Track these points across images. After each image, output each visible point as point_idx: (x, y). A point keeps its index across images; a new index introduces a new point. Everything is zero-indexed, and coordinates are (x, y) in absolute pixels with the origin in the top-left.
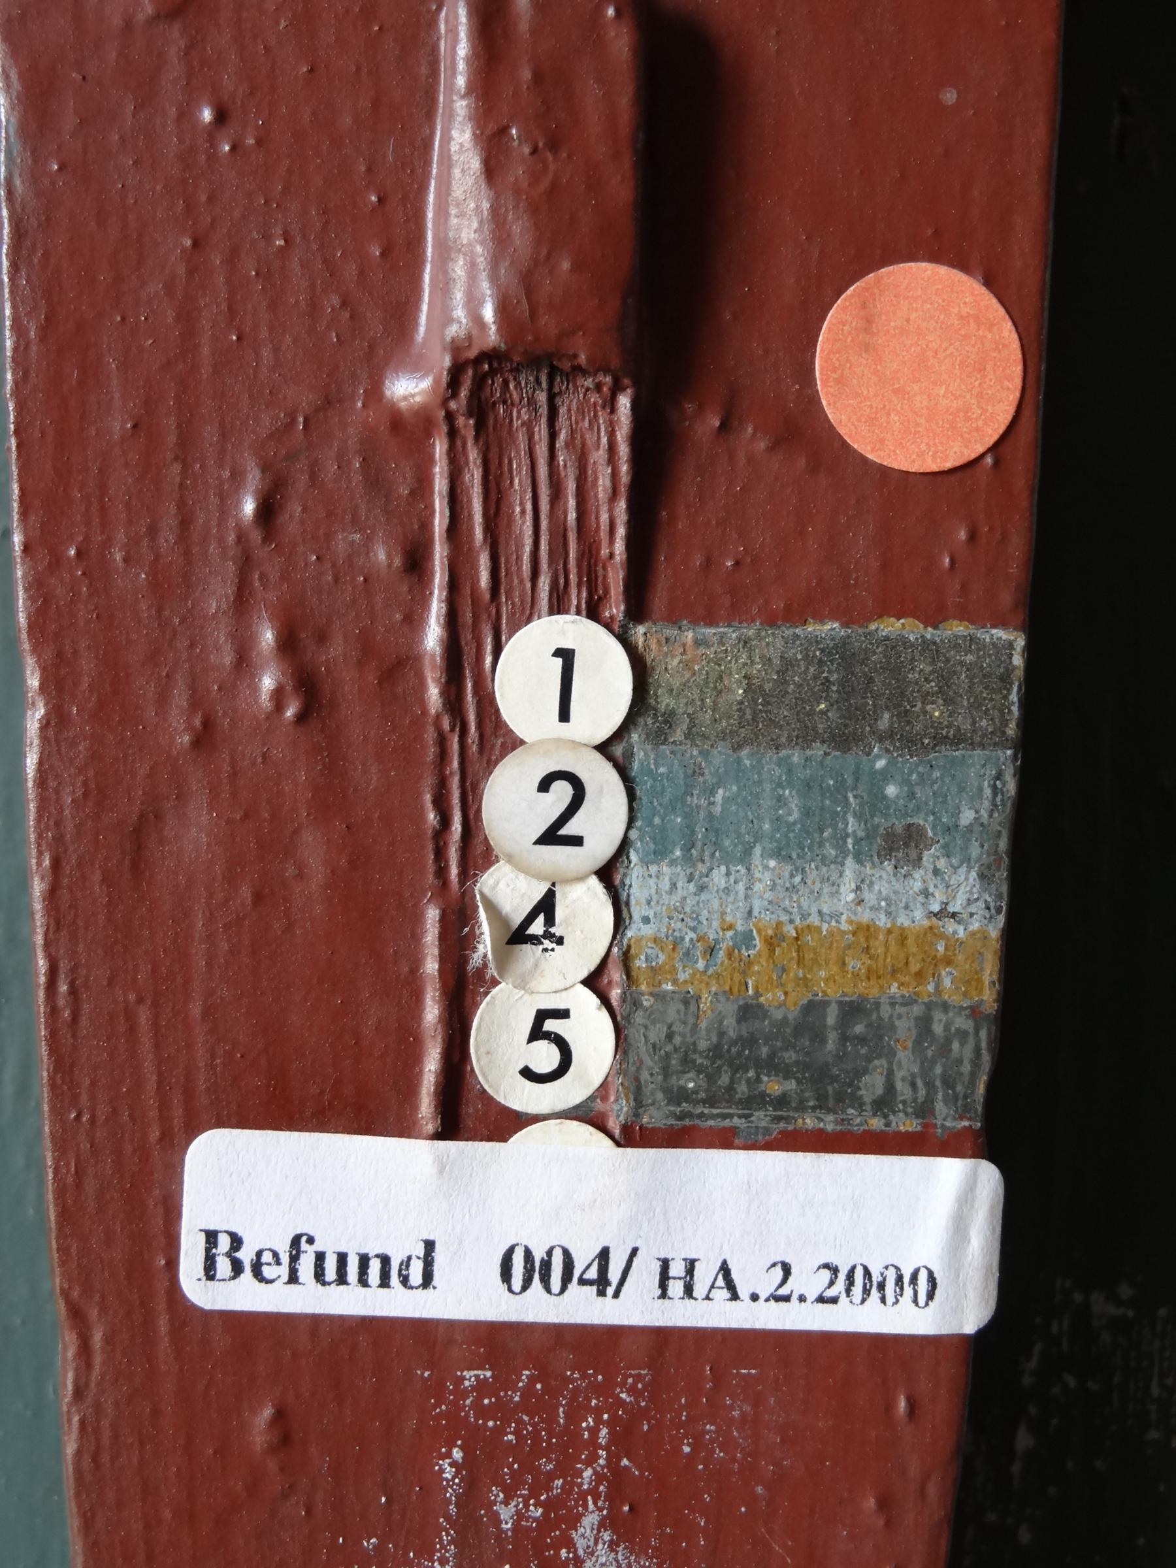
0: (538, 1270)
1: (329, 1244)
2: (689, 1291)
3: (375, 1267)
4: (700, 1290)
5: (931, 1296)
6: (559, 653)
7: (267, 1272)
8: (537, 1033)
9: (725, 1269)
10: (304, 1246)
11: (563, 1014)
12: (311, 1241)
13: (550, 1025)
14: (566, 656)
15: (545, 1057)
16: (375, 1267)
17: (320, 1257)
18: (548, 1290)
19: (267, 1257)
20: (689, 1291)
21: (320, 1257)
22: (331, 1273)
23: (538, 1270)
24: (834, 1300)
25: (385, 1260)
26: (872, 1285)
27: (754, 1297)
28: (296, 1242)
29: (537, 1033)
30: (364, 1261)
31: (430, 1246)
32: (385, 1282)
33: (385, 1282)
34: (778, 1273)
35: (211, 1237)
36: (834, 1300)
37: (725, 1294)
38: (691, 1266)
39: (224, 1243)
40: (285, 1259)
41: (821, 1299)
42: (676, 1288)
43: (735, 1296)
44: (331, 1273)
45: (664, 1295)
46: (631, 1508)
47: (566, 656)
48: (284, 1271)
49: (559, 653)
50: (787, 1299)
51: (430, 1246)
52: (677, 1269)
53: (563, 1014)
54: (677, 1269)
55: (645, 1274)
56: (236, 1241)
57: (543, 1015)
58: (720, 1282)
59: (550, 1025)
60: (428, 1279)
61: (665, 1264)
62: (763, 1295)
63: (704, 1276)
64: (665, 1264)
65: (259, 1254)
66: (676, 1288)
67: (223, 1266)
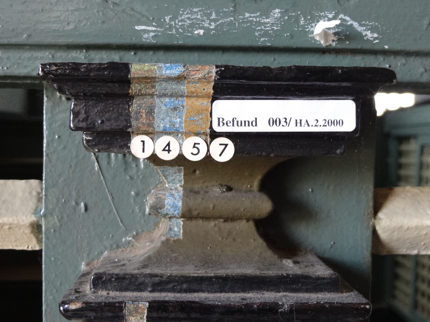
0: (275, 122)
1: (239, 119)
2: (301, 126)
3: (247, 123)
4: (303, 124)
5: (269, 120)
6: (142, 141)
7: (229, 124)
8: (194, 147)
9: (307, 121)
10: (235, 120)
11: (199, 144)
12: (236, 119)
13: (196, 146)
14: (143, 142)
15: (195, 151)
16: (247, 123)
17: (238, 121)
18: (276, 125)
19: (228, 122)
20: (301, 126)
21: (238, 121)
22: (239, 124)
23: (275, 122)
24: (326, 126)
25: (249, 122)
26: (333, 123)
27: (312, 126)
28: (233, 119)
29: (194, 147)
30: (241, 125)
31: (256, 119)
32: (249, 125)
33: (249, 125)
34: (316, 121)
35: (219, 119)
36: (326, 126)
37: (307, 125)
38: (301, 120)
39: (221, 120)
40: (232, 122)
41: (324, 126)
42: (299, 124)
43: (309, 126)
44: (239, 124)
45: (296, 125)
46: (54, 259)
47: (143, 142)
48: (231, 124)
49: (142, 141)
50: (317, 126)
51: (256, 119)
52: (299, 121)
53: (199, 144)
54: (299, 121)
55: (293, 123)
56: (223, 119)
57: (195, 144)
58: (306, 123)
59: (196, 146)
60: (256, 125)
61: (296, 120)
62: (314, 125)
63: (303, 122)
64: (296, 120)
65: (227, 122)
66: (299, 124)
67: (221, 124)
